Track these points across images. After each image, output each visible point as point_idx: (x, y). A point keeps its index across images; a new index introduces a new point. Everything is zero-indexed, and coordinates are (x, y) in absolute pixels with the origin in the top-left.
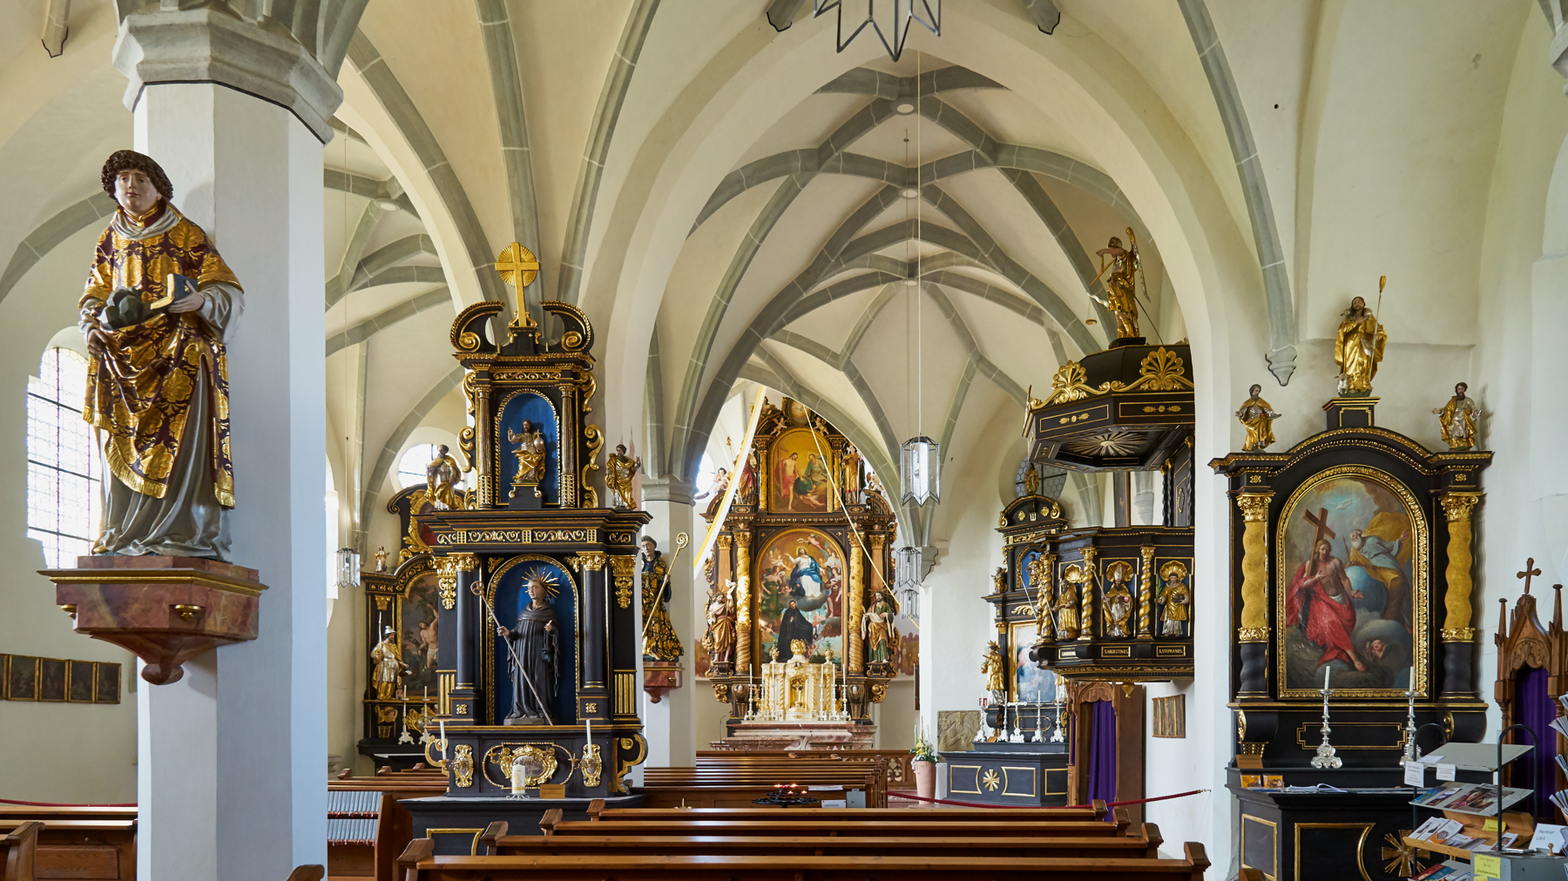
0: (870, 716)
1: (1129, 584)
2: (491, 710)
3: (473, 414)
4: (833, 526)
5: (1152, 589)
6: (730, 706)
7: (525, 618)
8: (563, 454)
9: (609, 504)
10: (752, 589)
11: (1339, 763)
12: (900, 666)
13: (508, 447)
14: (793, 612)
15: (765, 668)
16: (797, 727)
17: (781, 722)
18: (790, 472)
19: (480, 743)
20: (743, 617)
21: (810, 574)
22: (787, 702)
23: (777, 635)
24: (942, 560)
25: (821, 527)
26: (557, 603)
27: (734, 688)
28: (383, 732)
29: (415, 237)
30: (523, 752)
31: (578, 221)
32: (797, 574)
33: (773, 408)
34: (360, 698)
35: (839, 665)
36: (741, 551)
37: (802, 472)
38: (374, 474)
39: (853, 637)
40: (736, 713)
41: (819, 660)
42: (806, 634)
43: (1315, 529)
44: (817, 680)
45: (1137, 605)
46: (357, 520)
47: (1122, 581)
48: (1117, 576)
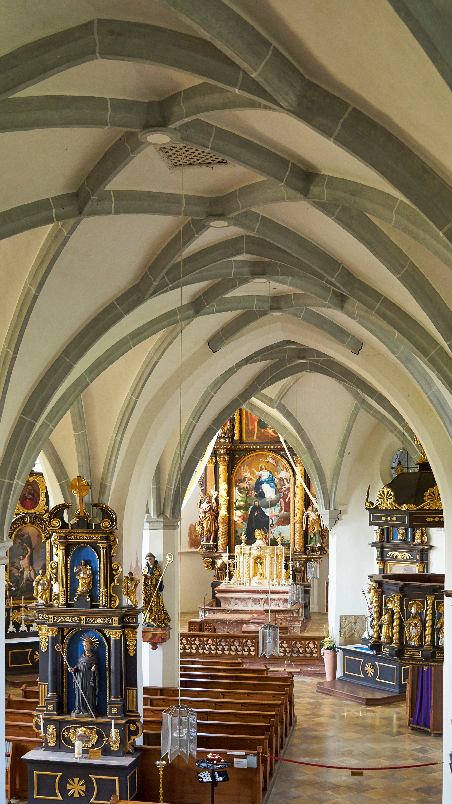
1: (420, 614)
2: (65, 709)
3: (57, 555)
5: (433, 620)
7: (82, 661)
8: (101, 577)
9: (124, 604)
10: (229, 493)
13: (74, 575)
14: (257, 508)
15: (237, 548)
16: (258, 592)
17: (246, 587)
19: (59, 725)
20: (223, 512)
21: (268, 483)
23: (246, 524)
24: (343, 517)
26: (97, 654)
30: (80, 731)
31: (110, 463)
32: (259, 483)
36: (222, 468)
39: (297, 527)
41: (274, 543)
45: (424, 628)
47: (417, 613)
48: (413, 611)
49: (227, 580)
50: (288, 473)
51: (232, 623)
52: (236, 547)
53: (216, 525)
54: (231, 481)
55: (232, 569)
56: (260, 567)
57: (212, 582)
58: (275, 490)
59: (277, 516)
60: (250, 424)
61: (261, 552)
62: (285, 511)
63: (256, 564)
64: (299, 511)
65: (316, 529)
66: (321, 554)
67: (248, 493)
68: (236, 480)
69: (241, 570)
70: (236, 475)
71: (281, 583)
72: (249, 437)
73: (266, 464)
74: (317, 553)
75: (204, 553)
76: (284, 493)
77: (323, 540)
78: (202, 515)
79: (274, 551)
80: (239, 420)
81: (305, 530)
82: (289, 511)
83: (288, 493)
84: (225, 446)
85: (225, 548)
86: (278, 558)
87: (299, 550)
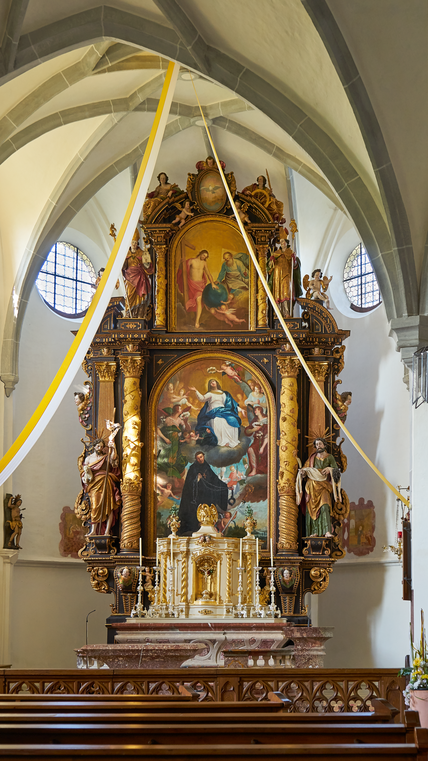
0: (306, 612)
4: (262, 348)
6: (111, 598)
10: (144, 434)
12: (346, 543)
14: (200, 467)
15: (161, 546)
16: (204, 627)
17: (182, 619)
18: (197, 276)
20: (130, 473)
21: (224, 415)
23: (178, 499)
25: (239, 350)
27: (117, 572)
33: (176, 191)
35: (264, 540)
36: (129, 383)
37: (215, 276)
39: (284, 501)
40: (120, 607)
41: (238, 533)
42: (220, 497)
44: (233, 561)
49: (139, 609)
50: (265, 397)
51: (152, 658)
52: (158, 541)
53: (117, 498)
54: (148, 410)
55: (149, 587)
56: (209, 581)
57: (108, 616)
58: (237, 429)
59: (242, 482)
60: (186, 298)
61: (211, 548)
62: (258, 472)
63: (200, 575)
64: (288, 468)
65: (322, 503)
66: (330, 556)
67: (183, 437)
68: (158, 410)
69: (169, 587)
70: (158, 400)
71: (252, 612)
72: (185, 324)
73: (219, 378)
74: (323, 554)
75: (91, 557)
76: (255, 437)
77: (335, 528)
78: (87, 477)
79: (237, 546)
80: (164, 287)
81: (299, 507)
82: (266, 473)
83: (263, 436)
84: (136, 336)
85: (135, 545)
86: (246, 564)
87: (287, 546)
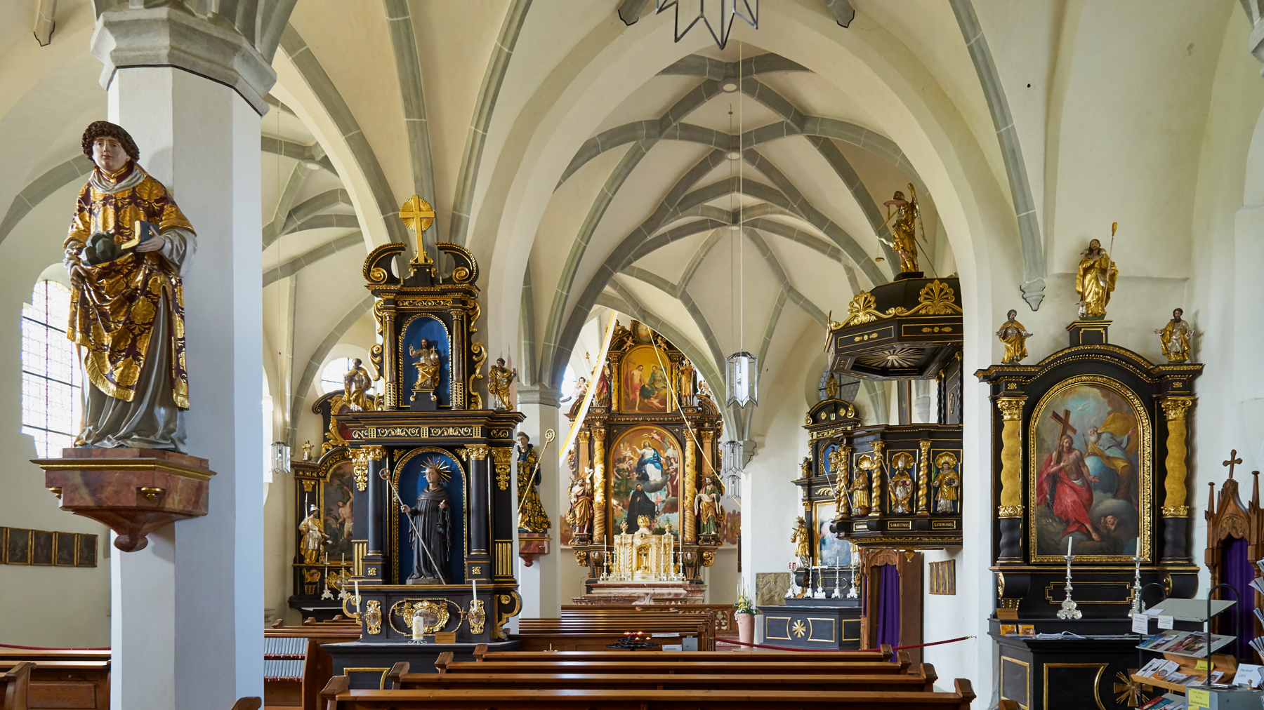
0: (701, 577)
1: (910, 471)
2: (395, 572)
3: (381, 333)
4: (672, 424)
5: (929, 475)
6: (588, 569)
7: (423, 498)
8: (454, 366)
9: (491, 406)
10: (606, 475)
11: (1079, 615)
12: (725, 537)
13: (410, 361)
14: (639, 493)
15: (617, 538)
16: (642, 586)
17: (629, 582)
18: (636, 380)
19: (387, 598)
20: (599, 498)
21: (653, 463)
22: (634, 566)
23: (626, 511)
24: (760, 451)
25: (662, 424)
26: (449, 486)
27: (592, 554)
28: (309, 590)
29: (335, 191)
30: (422, 606)
31: (466, 178)
32: (642, 463)
33: (623, 329)
34: (290, 562)
35: (676, 536)
36: (597, 444)
37: (647, 380)
38: (301, 382)
39: (688, 513)
40: (593, 574)
41: (661, 532)
42: (650, 511)
43: (1060, 426)
45: (916, 487)
46: (288, 419)
47: (905, 468)
